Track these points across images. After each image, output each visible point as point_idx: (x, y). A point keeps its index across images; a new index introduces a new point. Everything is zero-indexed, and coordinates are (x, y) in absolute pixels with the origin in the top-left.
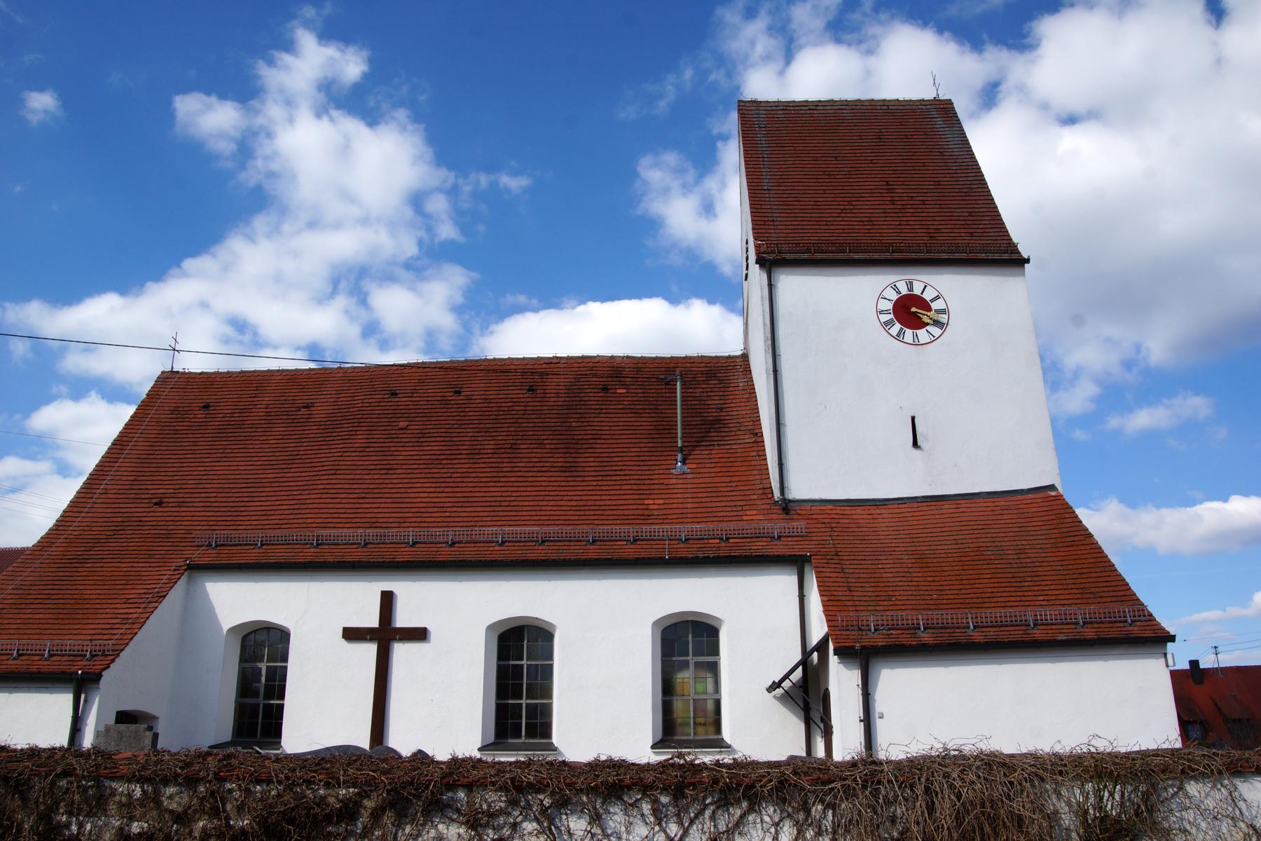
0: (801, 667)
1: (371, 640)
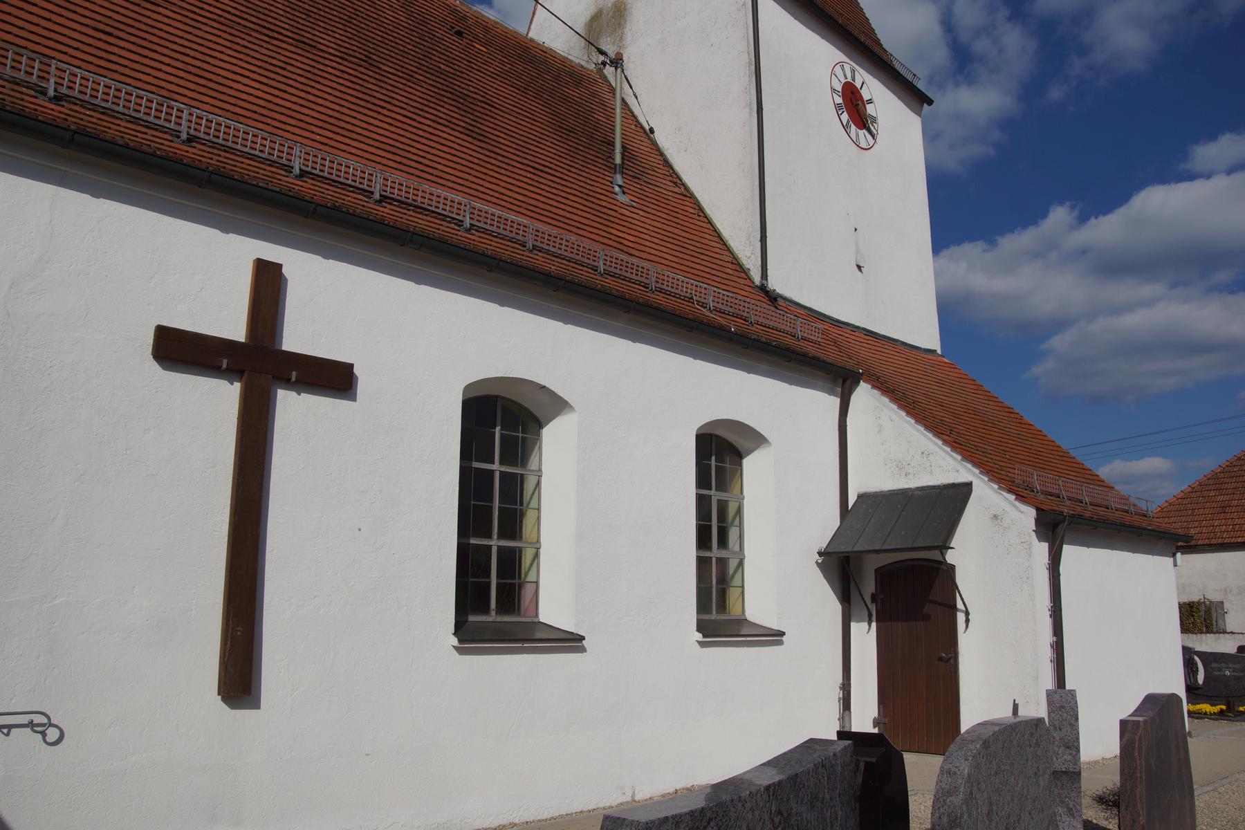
1: (230, 373)
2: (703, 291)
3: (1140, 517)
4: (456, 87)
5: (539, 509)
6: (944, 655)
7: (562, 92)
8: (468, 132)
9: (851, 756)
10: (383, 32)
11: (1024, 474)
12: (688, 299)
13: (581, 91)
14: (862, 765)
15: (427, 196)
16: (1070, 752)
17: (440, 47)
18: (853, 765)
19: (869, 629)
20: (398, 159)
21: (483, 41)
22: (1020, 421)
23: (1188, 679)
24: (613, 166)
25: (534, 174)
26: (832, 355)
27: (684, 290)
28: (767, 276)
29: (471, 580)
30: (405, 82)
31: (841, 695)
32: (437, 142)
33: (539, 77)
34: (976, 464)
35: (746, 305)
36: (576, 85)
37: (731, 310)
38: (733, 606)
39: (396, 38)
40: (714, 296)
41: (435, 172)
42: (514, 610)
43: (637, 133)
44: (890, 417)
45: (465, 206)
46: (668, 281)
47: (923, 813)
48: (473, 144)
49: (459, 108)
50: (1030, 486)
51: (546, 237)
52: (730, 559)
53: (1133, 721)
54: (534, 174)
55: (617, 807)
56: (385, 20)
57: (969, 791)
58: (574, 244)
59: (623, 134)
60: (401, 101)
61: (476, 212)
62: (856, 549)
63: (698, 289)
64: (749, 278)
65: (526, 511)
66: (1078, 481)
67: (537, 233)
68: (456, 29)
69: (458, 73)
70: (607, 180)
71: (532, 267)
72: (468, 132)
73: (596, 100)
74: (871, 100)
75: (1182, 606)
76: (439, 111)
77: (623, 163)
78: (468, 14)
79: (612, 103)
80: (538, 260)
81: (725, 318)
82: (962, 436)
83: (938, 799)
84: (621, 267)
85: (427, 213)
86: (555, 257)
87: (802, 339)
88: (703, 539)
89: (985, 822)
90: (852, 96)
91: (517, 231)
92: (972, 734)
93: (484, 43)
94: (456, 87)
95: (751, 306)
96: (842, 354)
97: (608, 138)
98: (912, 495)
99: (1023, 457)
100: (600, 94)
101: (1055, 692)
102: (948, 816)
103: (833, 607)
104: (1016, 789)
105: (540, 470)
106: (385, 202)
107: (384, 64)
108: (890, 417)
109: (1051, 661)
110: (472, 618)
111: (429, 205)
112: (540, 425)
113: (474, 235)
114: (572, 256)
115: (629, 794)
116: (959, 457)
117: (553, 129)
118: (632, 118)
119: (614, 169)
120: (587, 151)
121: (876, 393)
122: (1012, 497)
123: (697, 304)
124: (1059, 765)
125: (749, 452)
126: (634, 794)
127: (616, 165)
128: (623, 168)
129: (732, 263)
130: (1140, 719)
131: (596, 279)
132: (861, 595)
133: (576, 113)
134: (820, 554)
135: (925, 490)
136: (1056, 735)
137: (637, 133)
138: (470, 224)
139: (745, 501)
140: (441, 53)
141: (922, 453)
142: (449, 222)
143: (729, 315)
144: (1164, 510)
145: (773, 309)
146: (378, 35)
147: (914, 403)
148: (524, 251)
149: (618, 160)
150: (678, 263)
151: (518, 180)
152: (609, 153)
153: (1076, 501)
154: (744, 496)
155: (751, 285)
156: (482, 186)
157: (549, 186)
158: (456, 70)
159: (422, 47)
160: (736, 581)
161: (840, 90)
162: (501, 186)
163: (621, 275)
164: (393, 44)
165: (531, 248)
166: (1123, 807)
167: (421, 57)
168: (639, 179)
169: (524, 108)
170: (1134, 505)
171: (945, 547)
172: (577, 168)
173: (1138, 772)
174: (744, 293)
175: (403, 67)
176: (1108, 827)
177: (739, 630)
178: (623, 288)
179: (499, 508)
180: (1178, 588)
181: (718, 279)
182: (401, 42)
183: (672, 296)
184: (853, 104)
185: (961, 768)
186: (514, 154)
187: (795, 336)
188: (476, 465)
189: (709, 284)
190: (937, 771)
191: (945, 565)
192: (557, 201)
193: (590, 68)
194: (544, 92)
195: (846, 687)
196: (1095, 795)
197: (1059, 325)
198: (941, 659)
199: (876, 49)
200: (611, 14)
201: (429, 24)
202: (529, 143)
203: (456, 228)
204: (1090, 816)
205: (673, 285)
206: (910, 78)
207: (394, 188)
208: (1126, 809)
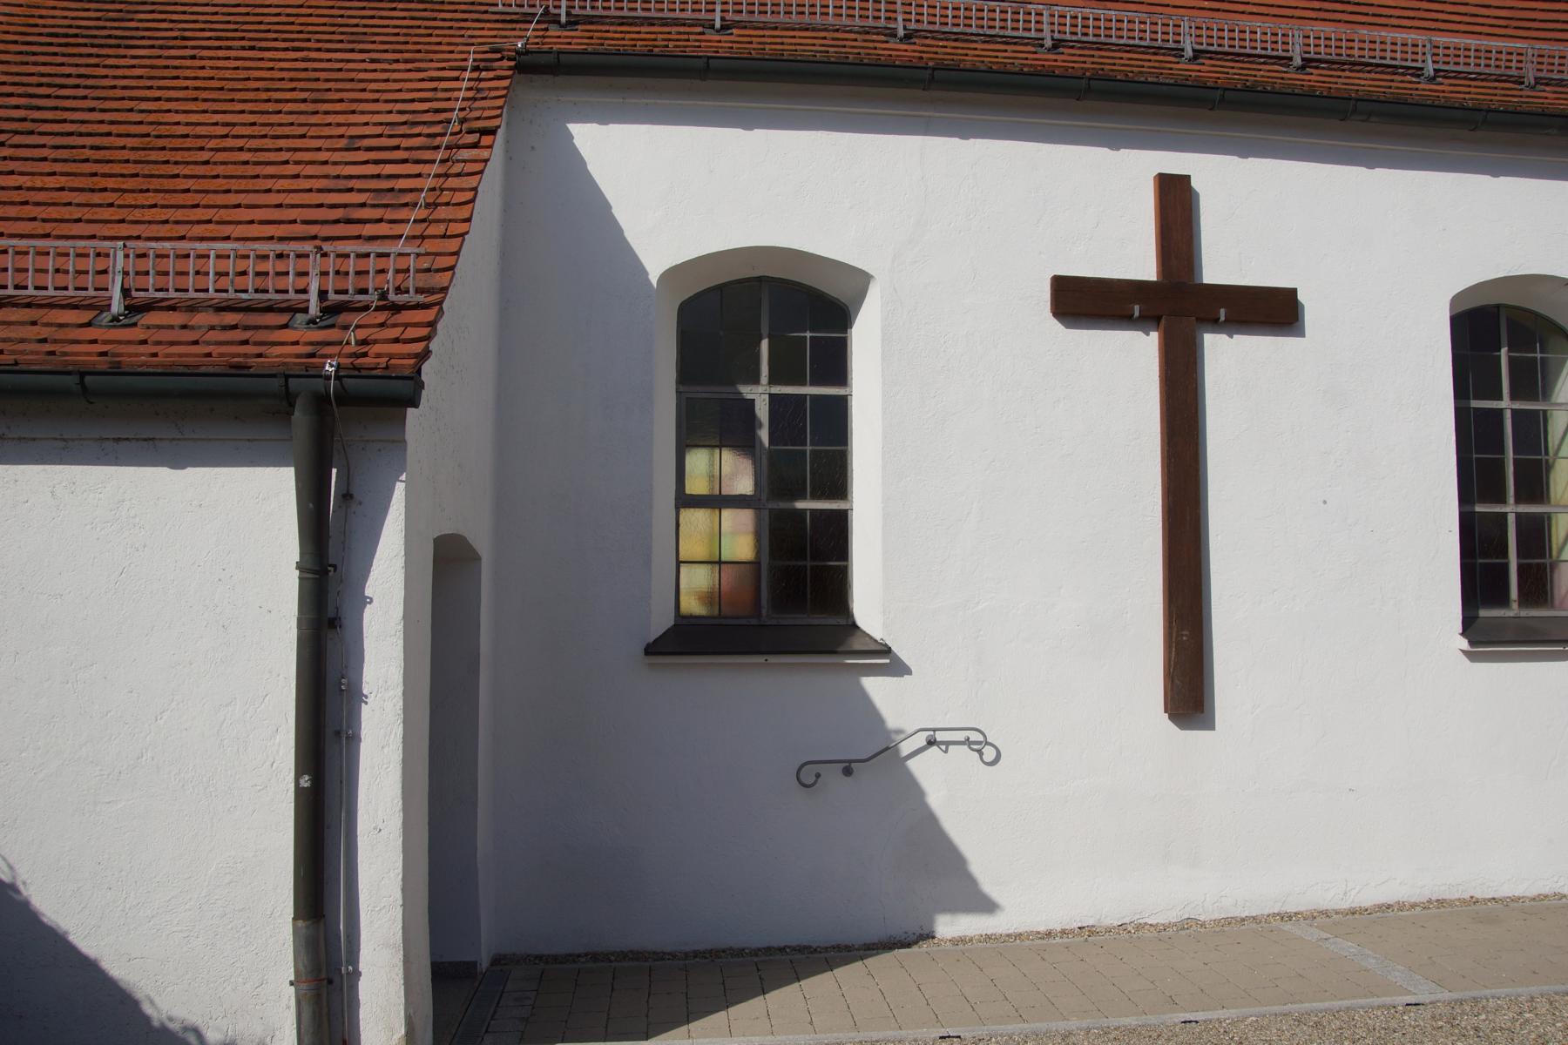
0: (574, 128)
1: (1145, 321)
29: (1481, 561)
42: (1546, 600)
45: (1424, 46)
67: (1540, 60)
80: (1546, 98)
85: (1369, 68)
91: (1508, 64)
110: (1483, 613)
142: (1403, 74)
148: (1521, 90)
156: (1442, 12)
165: (1532, 82)
188: (1475, 404)
203: (1414, 79)
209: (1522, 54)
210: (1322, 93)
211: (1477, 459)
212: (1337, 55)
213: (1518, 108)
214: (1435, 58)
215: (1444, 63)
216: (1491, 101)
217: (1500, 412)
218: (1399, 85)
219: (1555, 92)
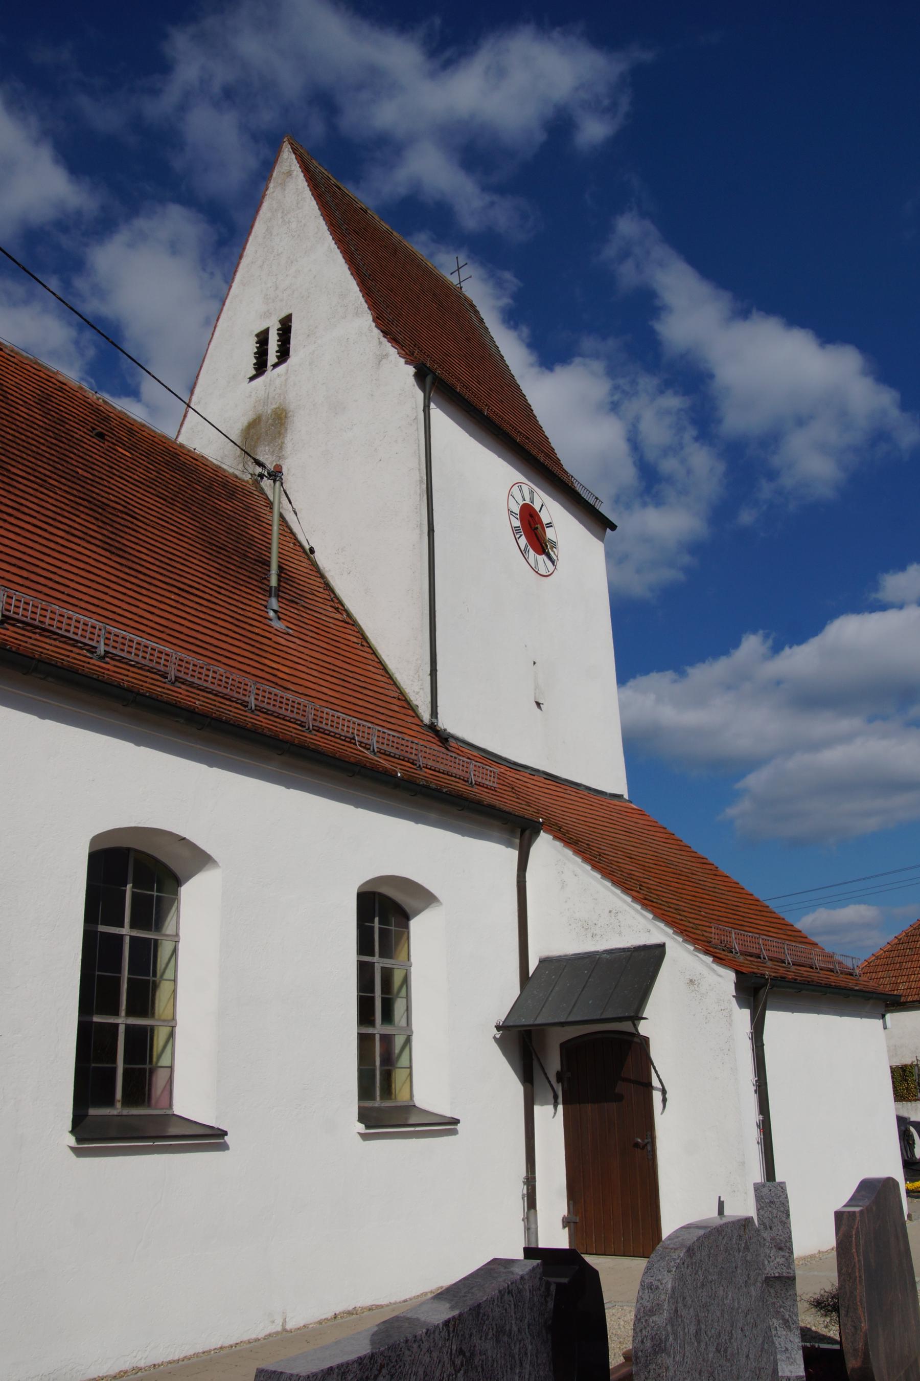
2: (366, 730)
3: (847, 976)
4: (94, 495)
5: (175, 981)
6: (639, 1140)
7: (214, 505)
8: (106, 546)
9: (541, 1279)
10: (14, 430)
11: (722, 933)
12: (349, 740)
13: (234, 504)
14: (553, 1288)
15: (57, 617)
16: (783, 1254)
17: (79, 450)
18: (543, 1289)
19: (555, 1113)
20: (25, 574)
21: (127, 444)
22: (715, 872)
23: (905, 1154)
24: (268, 588)
25: (179, 595)
26: (509, 802)
27: (345, 729)
28: (437, 714)
29: (93, 1065)
30: (36, 486)
31: (525, 1192)
32: (70, 556)
33: (188, 486)
34: (670, 923)
35: (414, 746)
36: (229, 497)
37: (398, 752)
38: (400, 1091)
39: (29, 437)
40: (378, 736)
41: (67, 591)
42: (144, 1101)
43: (295, 552)
44: (574, 872)
45: (100, 630)
46: (327, 719)
47: (623, 1329)
48: (110, 559)
49: (97, 519)
50: (728, 946)
51: (191, 667)
52: (396, 1036)
53: (849, 1212)
54: (179, 595)
55: (265, 1339)
56: (18, 418)
57: (673, 1307)
58: (222, 676)
59: (280, 553)
60: (31, 509)
61: (112, 637)
62: (539, 1021)
63: (361, 728)
64: (417, 716)
65: (160, 982)
66: (779, 938)
67: (181, 663)
68: (97, 431)
69: (98, 480)
70: (261, 604)
71: (174, 702)
72: (106, 546)
73: (252, 514)
74: (550, 523)
75: (894, 1070)
76: (74, 521)
77: (279, 585)
78: (112, 415)
79: (269, 518)
80: (181, 694)
81: (390, 761)
82: (653, 891)
83: (640, 1320)
84: (275, 703)
85: (55, 637)
86: (200, 690)
87: (476, 784)
88: (365, 1014)
89: (693, 1344)
90: (530, 518)
91: (158, 660)
92: (675, 1240)
93: (128, 447)
94: (94, 495)
95: (420, 748)
96: (521, 802)
97: (264, 557)
98: (599, 958)
99: (719, 914)
100: (256, 508)
101: (764, 1186)
102: (652, 1339)
103: (515, 1089)
104: (725, 1302)
105: (177, 935)
106: (8, 624)
107: (14, 466)
108: (574, 872)
109: (758, 1143)
110: (92, 1112)
111: (58, 628)
112: (178, 882)
113: (109, 663)
114: (219, 689)
115: (279, 1322)
116: (650, 916)
117: (202, 545)
118: (291, 535)
119: (269, 592)
120: (240, 570)
121: (559, 844)
122: (709, 960)
123: (360, 745)
124: (772, 1270)
125: (417, 912)
126: (285, 1321)
127: (271, 587)
128: (279, 590)
129: (399, 699)
130: (857, 1209)
131: (246, 717)
132: (545, 1074)
133: (228, 528)
134: (498, 1028)
135: (614, 953)
136: (766, 1235)
137: (295, 552)
138: (105, 651)
139: (412, 968)
140: (80, 456)
141: (610, 912)
142: (81, 648)
143: (394, 757)
144: (871, 965)
145: (444, 750)
146: (9, 433)
147: (600, 855)
148: (165, 683)
149: (274, 582)
150: (338, 698)
151: (161, 602)
152: (264, 573)
153: (777, 962)
154: (411, 963)
155: (420, 723)
156: (120, 607)
157: (196, 609)
158: (96, 476)
159: (58, 449)
160: (403, 1061)
161: (518, 512)
162: (141, 609)
163: (274, 712)
164: (25, 444)
165: (173, 679)
166: (843, 1312)
167: (57, 460)
168: (297, 603)
169: (169, 520)
170: (839, 963)
171: (637, 1017)
172: (227, 590)
173: (857, 1270)
174: (412, 733)
175: (35, 470)
176: (829, 1335)
177: (407, 1119)
178: (276, 727)
179: (129, 979)
180: (889, 1051)
181: (383, 717)
182: (34, 443)
183: (332, 736)
184: (531, 527)
185: (664, 1282)
186: (157, 572)
187: (468, 782)
188: (102, 928)
189: (373, 723)
190: (637, 1286)
191: (637, 1037)
192: (204, 627)
193: (246, 479)
194: (194, 503)
195: (530, 1181)
196: (812, 1300)
197: (751, 764)
198: (636, 1145)
199: (556, 470)
200: (270, 421)
201: (67, 424)
202: (174, 561)
203: (88, 655)
204: (809, 1323)
205: (332, 724)
206: (591, 501)
207: (19, 607)
208: (847, 1315)
209: (169, 655)
210: (11, 648)
211: (98, 975)
212: (31, 618)
213: (159, 697)
214: (107, 641)
215: (113, 647)
216: (142, 686)
217: (121, 937)
218: (74, 657)
219: (187, 691)
